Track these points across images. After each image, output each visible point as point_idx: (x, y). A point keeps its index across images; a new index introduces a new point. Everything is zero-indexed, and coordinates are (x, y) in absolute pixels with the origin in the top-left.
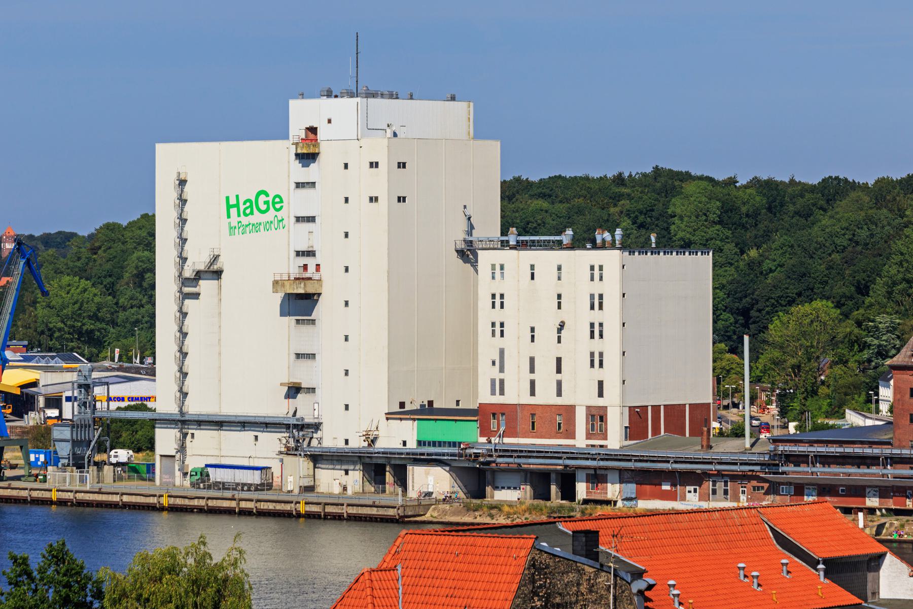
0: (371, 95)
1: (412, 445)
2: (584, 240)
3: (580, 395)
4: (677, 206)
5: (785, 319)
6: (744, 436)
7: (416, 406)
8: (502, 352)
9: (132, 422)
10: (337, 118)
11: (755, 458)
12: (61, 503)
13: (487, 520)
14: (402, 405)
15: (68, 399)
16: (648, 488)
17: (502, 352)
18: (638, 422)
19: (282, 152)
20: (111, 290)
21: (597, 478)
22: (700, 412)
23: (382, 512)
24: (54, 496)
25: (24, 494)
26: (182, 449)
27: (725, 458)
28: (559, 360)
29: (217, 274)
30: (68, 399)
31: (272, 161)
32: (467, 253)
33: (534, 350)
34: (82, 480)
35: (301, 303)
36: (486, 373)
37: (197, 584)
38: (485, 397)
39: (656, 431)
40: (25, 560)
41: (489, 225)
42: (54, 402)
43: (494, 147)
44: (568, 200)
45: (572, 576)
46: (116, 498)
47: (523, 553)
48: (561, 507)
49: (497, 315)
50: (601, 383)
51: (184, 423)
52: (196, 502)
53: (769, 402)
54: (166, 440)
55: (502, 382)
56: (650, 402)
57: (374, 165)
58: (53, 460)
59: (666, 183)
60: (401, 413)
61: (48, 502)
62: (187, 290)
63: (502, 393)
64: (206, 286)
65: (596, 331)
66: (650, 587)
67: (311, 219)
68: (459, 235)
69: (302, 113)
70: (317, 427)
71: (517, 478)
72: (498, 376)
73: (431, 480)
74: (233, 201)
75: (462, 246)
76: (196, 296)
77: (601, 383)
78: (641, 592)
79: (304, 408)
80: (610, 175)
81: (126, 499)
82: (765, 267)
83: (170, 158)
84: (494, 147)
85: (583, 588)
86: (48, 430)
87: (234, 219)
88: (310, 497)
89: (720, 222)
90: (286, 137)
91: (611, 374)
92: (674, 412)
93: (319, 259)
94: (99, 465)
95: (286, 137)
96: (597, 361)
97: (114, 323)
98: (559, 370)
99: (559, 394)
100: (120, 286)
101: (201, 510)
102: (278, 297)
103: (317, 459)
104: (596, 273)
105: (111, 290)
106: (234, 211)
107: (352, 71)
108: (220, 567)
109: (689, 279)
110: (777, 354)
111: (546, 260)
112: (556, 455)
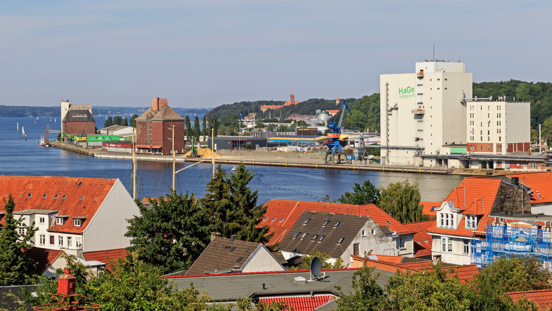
0: (437, 61)
1: (449, 154)
2: (495, 99)
3: (494, 141)
4: (517, 89)
5: (548, 119)
6: (176, 164)
7: (450, 144)
8: (473, 129)
9: (374, 148)
10: (429, 67)
11: (542, 157)
12: (356, 169)
13: (470, 174)
14: (446, 143)
15: (357, 142)
16: (513, 165)
17: (473, 129)
18: (510, 148)
19: (415, 76)
20: (366, 113)
21: (499, 162)
22: (527, 145)
23: (441, 172)
24: (354, 168)
25: (346, 167)
26: (388, 155)
27: (534, 157)
28: (489, 131)
29: (397, 109)
30: (357, 142)
31: (411, 79)
32: (464, 103)
33: (482, 128)
34: (361, 163)
35: (419, 116)
36: (469, 135)
37: (406, 191)
38: (469, 141)
39: (515, 150)
40: (359, 185)
41: (470, 95)
42: (353, 143)
43: (471, 75)
44: (487, 88)
45: (512, 190)
46: (370, 168)
47: (499, 183)
48: (489, 171)
49: (472, 119)
50: (500, 137)
51: (388, 148)
52: (391, 169)
53: (544, 142)
54: (383, 153)
56: (513, 142)
57: (438, 80)
58: (353, 158)
59: (515, 84)
60: (446, 145)
61: (352, 169)
62: (389, 113)
64: (394, 112)
65: (498, 123)
66: (532, 193)
67: (422, 94)
68: (461, 98)
69: (419, 66)
70: (424, 149)
71: (477, 162)
72: (472, 136)
73: (454, 163)
75: (462, 101)
76: (391, 115)
77: (500, 137)
78: (529, 194)
79: (420, 144)
80: (499, 82)
81: (373, 168)
82: (542, 106)
83: (384, 78)
84: (471, 75)
85: (515, 193)
86: (352, 150)
88: (422, 168)
89: (529, 94)
90: (414, 72)
91: (503, 135)
92: (520, 145)
93: (424, 105)
94: (366, 159)
95: (414, 72)
96: (499, 131)
97: (367, 122)
98: (482, 137)
99: (489, 140)
100: (368, 112)
101: (393, 171)
102: (413, 115)
103: (423, 158)
104: (499, 108)
105: (366, 113)
106: (401, 92)
107: (432, 55)
108: (412, 187)
109: (524, 109)
110: (547, 129)
111: (485, 104)
112: (488, 157)
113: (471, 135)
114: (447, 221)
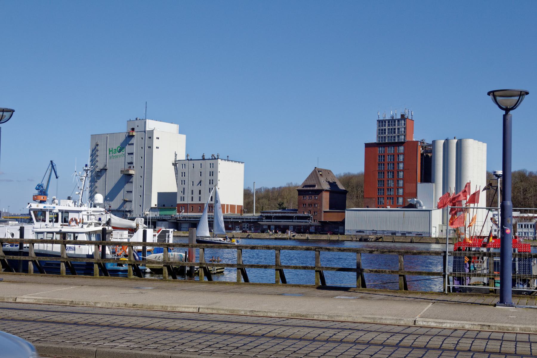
8: (184, 189)
17: (184, 189)
55: (184, 197)
56: (226, 203)
63: (184, 200)
72: (183, 196)
74: (111, 150)
75: (174, 162)
87: (111, 155)
93: (134, 165)
98: (200, 194)
99: (200, 200)
106: (111, 152)
113: (182, 195)
114: (449, 284)
